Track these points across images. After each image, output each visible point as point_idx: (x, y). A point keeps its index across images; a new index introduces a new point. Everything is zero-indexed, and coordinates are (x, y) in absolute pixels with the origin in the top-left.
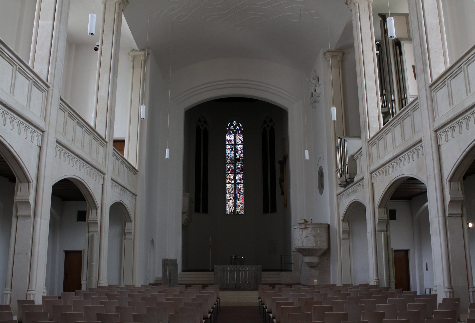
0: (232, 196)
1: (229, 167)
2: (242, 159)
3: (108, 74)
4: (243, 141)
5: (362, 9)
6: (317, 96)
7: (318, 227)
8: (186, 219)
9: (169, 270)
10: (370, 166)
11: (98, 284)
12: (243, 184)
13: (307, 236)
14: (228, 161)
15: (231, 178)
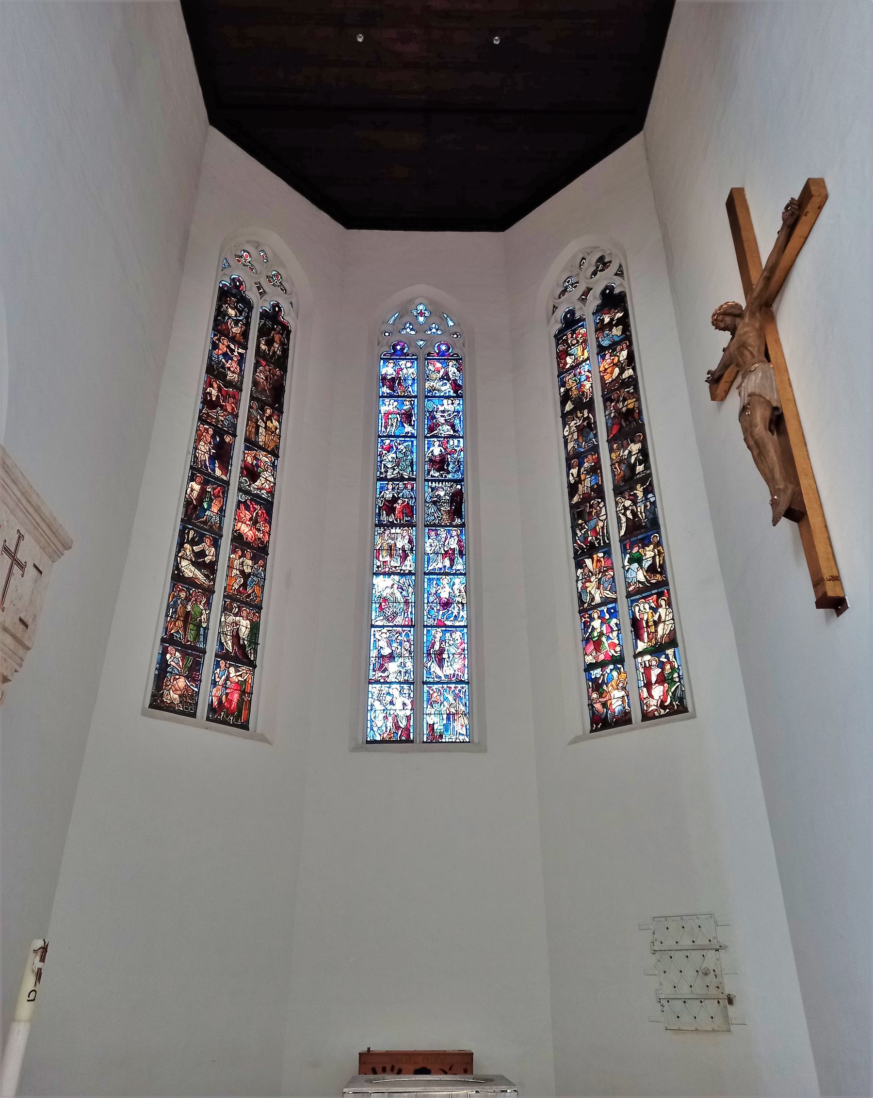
0: (403, 637)
15: (400, 545)
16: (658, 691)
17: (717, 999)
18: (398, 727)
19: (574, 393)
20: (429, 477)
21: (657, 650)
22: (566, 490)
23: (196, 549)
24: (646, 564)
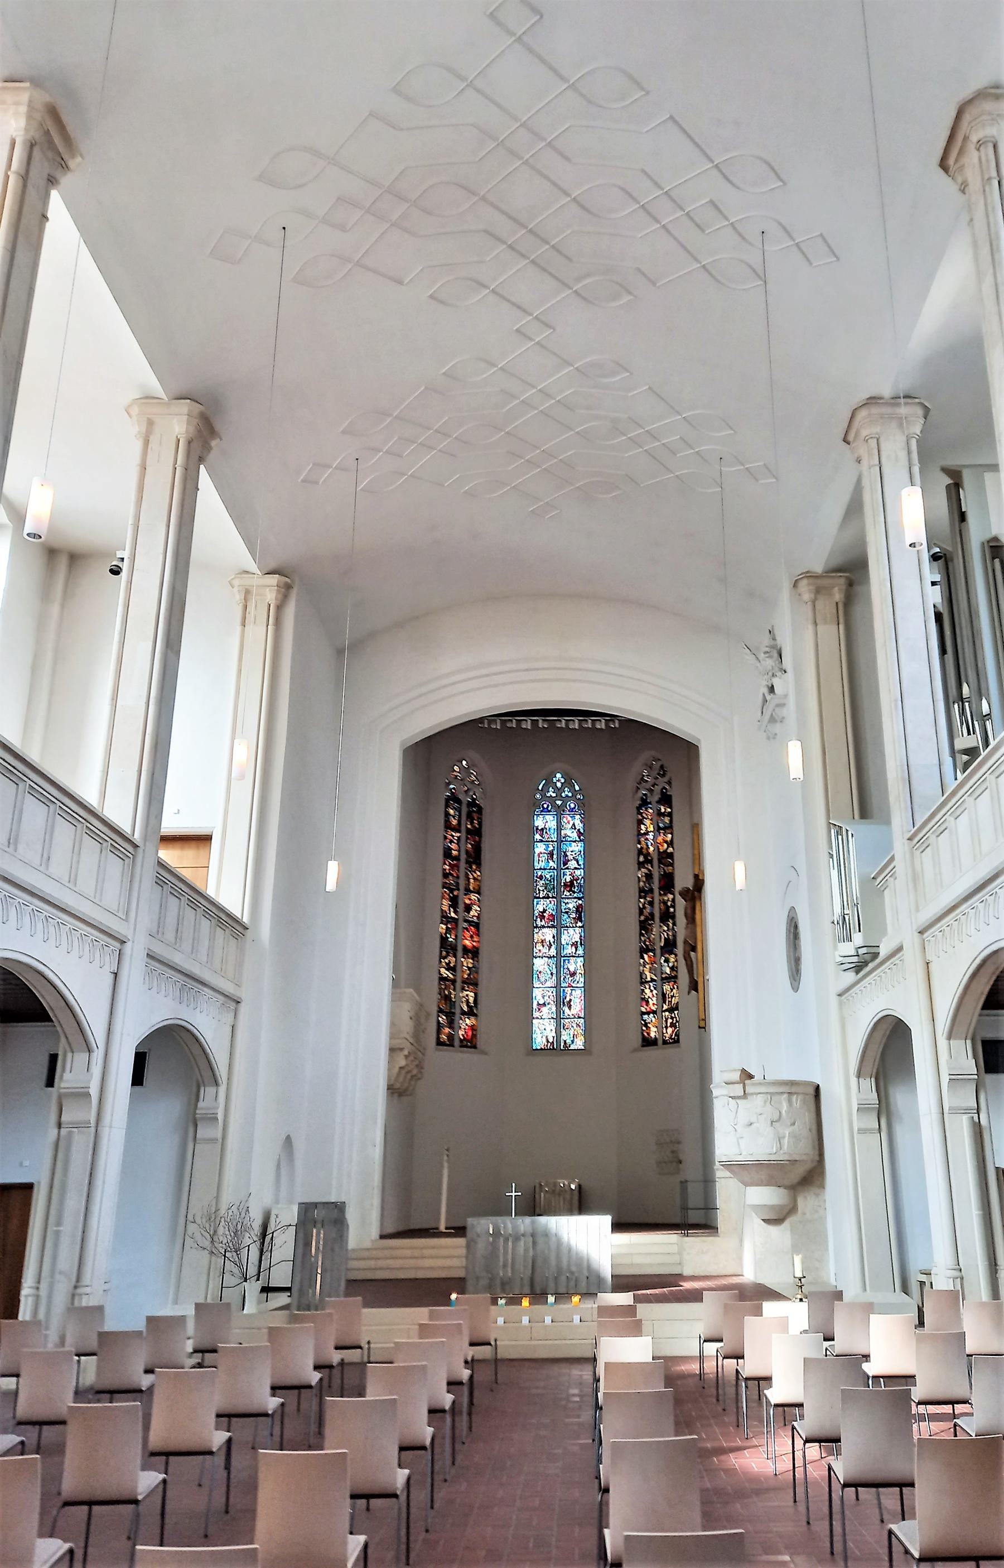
0: (550, 993)
1: (540, 908)
3: (150, 644)
4: (582, 831)
6: (779, 705)
8: (401, 1068)
9: (318, 1237)
10: (917, 910)
11: (73, 1296)
12: (582, 959)
13: (752, 1121)
14: (539, 890)
15: (547, 940)
16: (670, 1030)
18: (548, 1041)
19: (644, 851)
20: (564, 896)
21: (671, 1010)
22: (638, 911)
23: (447, 961)
24: (671, 965)
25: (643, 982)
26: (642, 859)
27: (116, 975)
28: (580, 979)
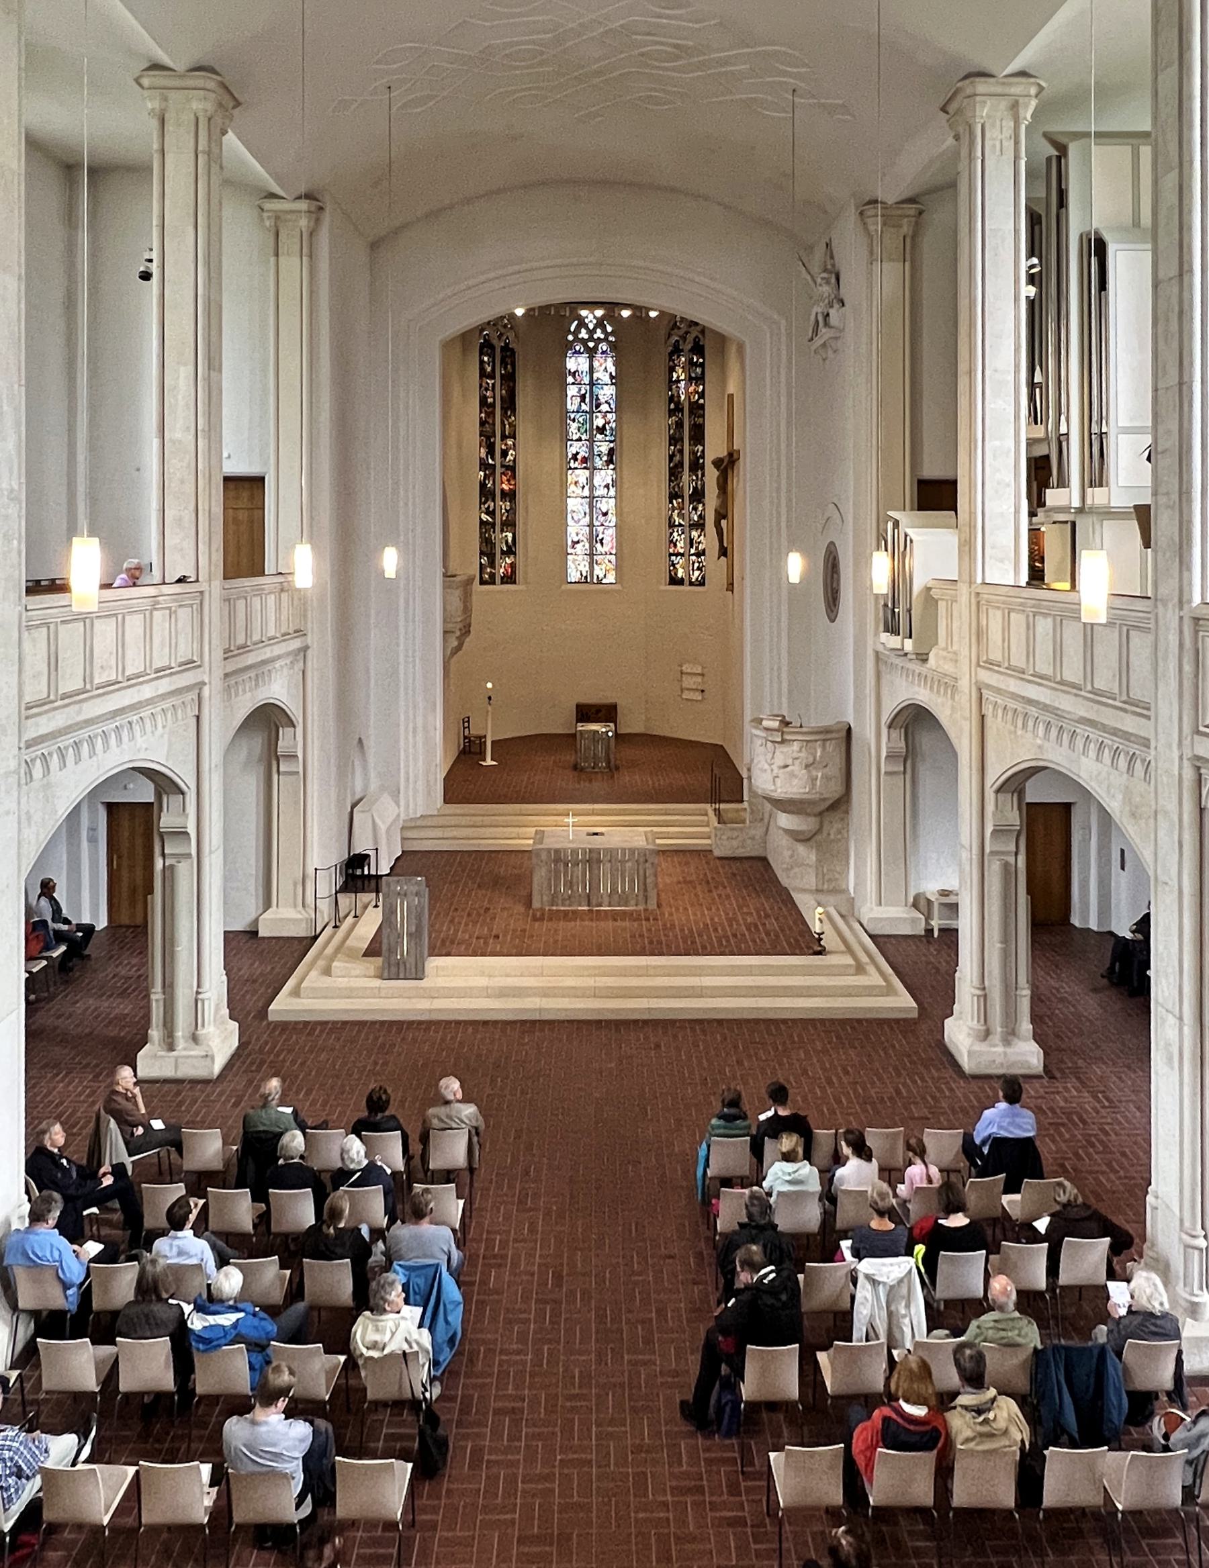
2: (611, 429)
3: (191, 368)
5: (994, 146)
7: (816, 741)
16: (697, 573)
17: (1156, 595)
21: (698, 555)
25: (672, 525)
26: (672, 406)
27: (198, 717)
28: (612, 518)
